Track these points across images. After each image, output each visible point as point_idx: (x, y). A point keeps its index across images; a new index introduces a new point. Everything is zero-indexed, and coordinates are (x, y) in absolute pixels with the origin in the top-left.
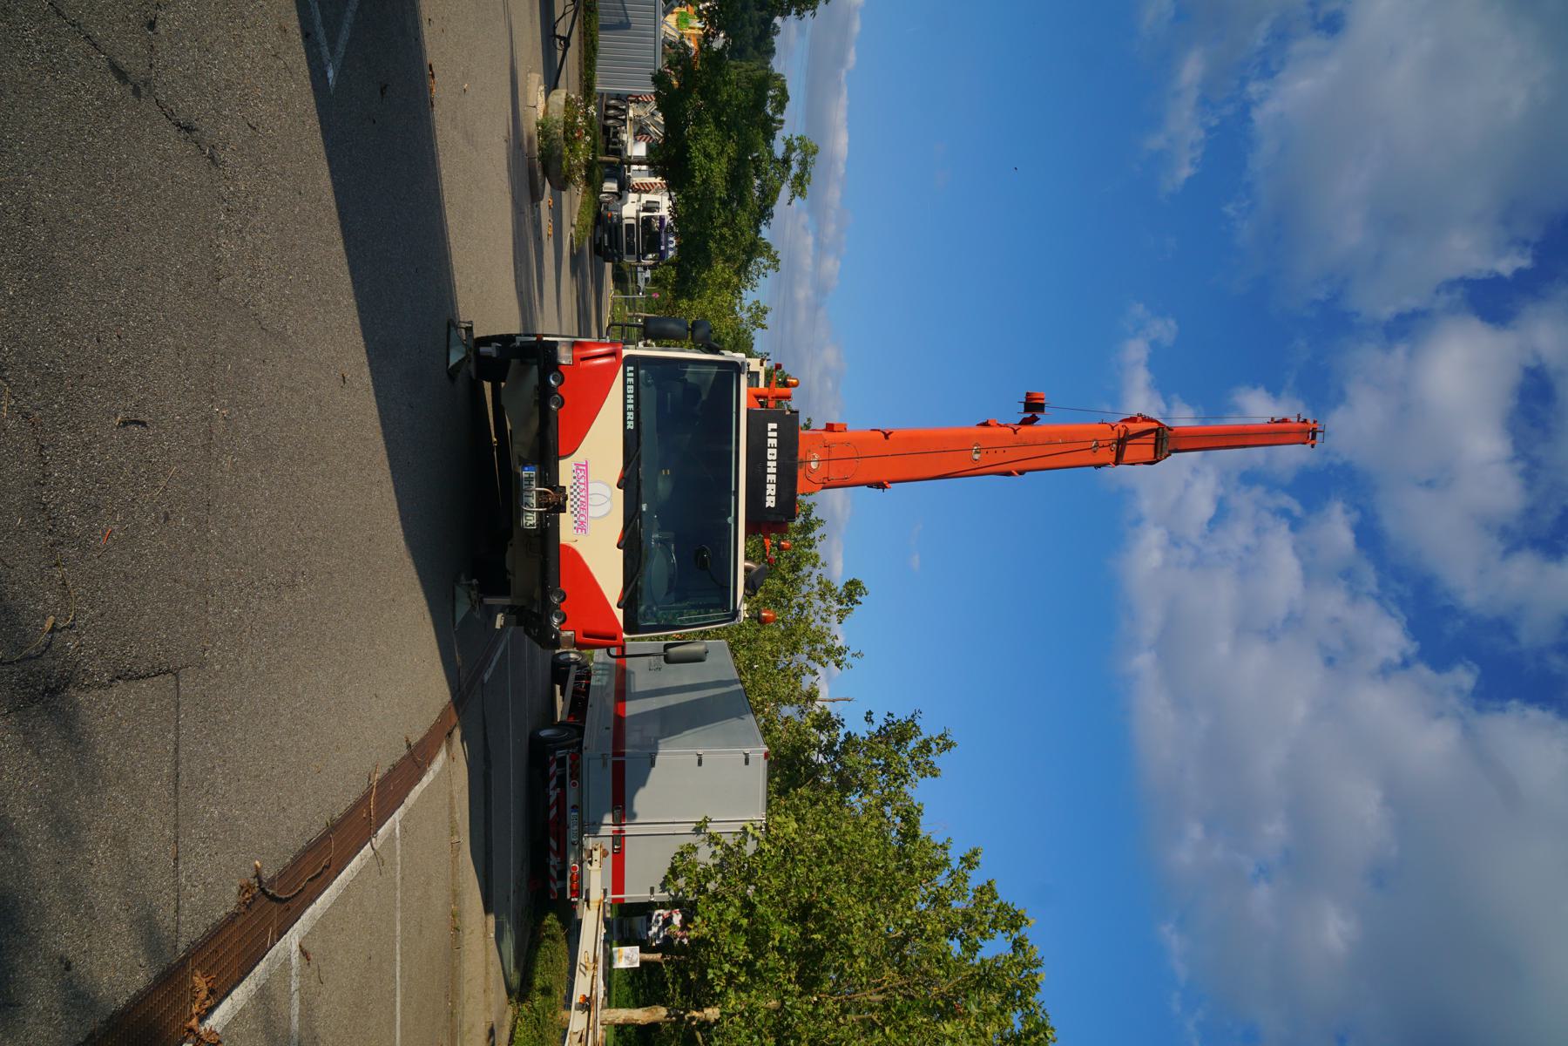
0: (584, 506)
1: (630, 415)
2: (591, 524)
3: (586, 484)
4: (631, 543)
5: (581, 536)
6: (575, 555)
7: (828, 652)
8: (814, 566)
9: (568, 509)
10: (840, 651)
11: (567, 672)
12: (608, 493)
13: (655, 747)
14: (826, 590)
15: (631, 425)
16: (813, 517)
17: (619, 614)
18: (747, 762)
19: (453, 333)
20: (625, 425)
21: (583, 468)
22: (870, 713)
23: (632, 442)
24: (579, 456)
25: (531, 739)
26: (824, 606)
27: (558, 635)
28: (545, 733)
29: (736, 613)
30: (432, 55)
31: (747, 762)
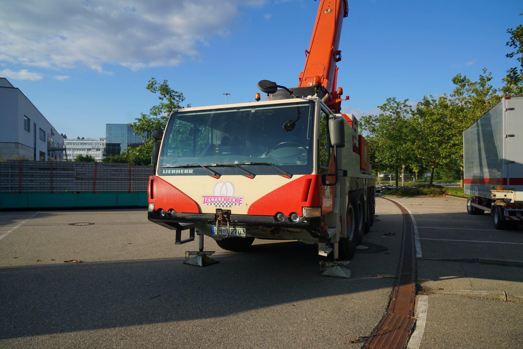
0: (227, 198)
1: (186, 171)
2: (238, 195)
3: (222, 197)
4: (251, 171)
5: (244, 202)
6: (254, 206)
7: (483, 85)
8: (446, 99)
9: (228, 208)
10: (482, 79)
11: (475, 208)
12: (220, 185)
13: (502, 160)
14: (458, 92)
15: (191, 171)
16: (423, 102)
17: (295, 177)
18: (512, 109)
19: (190, 262)
20: (191, 174)
21: (207, 199)
22: (507, 56)
23: (198, 170)
24: (200, 202)
25: (498, 229)
26: (466, 93)
27: (306, 219)
28: (496, 220)
29: (312, 102)
30: (60, 261)
31: (512, 109)
